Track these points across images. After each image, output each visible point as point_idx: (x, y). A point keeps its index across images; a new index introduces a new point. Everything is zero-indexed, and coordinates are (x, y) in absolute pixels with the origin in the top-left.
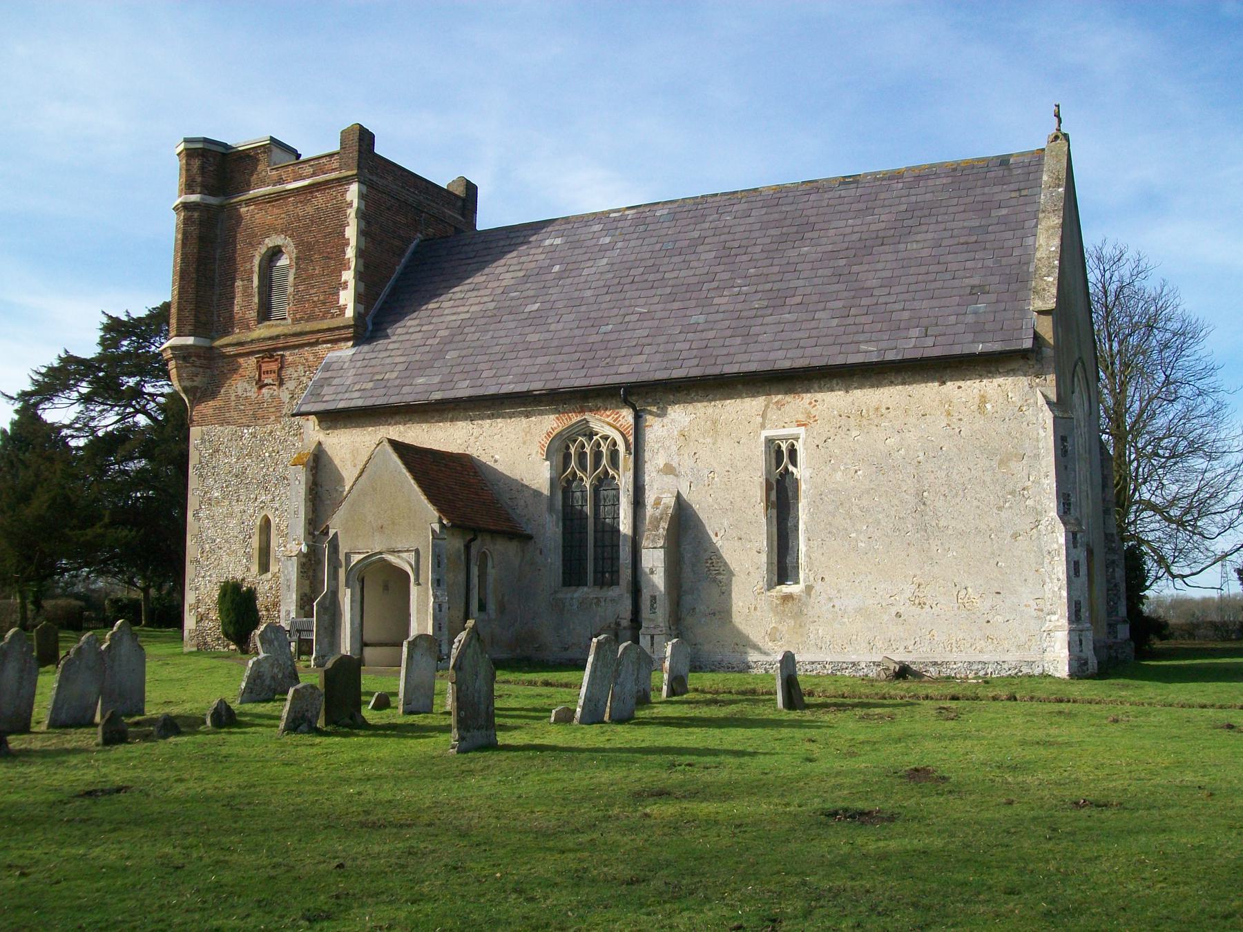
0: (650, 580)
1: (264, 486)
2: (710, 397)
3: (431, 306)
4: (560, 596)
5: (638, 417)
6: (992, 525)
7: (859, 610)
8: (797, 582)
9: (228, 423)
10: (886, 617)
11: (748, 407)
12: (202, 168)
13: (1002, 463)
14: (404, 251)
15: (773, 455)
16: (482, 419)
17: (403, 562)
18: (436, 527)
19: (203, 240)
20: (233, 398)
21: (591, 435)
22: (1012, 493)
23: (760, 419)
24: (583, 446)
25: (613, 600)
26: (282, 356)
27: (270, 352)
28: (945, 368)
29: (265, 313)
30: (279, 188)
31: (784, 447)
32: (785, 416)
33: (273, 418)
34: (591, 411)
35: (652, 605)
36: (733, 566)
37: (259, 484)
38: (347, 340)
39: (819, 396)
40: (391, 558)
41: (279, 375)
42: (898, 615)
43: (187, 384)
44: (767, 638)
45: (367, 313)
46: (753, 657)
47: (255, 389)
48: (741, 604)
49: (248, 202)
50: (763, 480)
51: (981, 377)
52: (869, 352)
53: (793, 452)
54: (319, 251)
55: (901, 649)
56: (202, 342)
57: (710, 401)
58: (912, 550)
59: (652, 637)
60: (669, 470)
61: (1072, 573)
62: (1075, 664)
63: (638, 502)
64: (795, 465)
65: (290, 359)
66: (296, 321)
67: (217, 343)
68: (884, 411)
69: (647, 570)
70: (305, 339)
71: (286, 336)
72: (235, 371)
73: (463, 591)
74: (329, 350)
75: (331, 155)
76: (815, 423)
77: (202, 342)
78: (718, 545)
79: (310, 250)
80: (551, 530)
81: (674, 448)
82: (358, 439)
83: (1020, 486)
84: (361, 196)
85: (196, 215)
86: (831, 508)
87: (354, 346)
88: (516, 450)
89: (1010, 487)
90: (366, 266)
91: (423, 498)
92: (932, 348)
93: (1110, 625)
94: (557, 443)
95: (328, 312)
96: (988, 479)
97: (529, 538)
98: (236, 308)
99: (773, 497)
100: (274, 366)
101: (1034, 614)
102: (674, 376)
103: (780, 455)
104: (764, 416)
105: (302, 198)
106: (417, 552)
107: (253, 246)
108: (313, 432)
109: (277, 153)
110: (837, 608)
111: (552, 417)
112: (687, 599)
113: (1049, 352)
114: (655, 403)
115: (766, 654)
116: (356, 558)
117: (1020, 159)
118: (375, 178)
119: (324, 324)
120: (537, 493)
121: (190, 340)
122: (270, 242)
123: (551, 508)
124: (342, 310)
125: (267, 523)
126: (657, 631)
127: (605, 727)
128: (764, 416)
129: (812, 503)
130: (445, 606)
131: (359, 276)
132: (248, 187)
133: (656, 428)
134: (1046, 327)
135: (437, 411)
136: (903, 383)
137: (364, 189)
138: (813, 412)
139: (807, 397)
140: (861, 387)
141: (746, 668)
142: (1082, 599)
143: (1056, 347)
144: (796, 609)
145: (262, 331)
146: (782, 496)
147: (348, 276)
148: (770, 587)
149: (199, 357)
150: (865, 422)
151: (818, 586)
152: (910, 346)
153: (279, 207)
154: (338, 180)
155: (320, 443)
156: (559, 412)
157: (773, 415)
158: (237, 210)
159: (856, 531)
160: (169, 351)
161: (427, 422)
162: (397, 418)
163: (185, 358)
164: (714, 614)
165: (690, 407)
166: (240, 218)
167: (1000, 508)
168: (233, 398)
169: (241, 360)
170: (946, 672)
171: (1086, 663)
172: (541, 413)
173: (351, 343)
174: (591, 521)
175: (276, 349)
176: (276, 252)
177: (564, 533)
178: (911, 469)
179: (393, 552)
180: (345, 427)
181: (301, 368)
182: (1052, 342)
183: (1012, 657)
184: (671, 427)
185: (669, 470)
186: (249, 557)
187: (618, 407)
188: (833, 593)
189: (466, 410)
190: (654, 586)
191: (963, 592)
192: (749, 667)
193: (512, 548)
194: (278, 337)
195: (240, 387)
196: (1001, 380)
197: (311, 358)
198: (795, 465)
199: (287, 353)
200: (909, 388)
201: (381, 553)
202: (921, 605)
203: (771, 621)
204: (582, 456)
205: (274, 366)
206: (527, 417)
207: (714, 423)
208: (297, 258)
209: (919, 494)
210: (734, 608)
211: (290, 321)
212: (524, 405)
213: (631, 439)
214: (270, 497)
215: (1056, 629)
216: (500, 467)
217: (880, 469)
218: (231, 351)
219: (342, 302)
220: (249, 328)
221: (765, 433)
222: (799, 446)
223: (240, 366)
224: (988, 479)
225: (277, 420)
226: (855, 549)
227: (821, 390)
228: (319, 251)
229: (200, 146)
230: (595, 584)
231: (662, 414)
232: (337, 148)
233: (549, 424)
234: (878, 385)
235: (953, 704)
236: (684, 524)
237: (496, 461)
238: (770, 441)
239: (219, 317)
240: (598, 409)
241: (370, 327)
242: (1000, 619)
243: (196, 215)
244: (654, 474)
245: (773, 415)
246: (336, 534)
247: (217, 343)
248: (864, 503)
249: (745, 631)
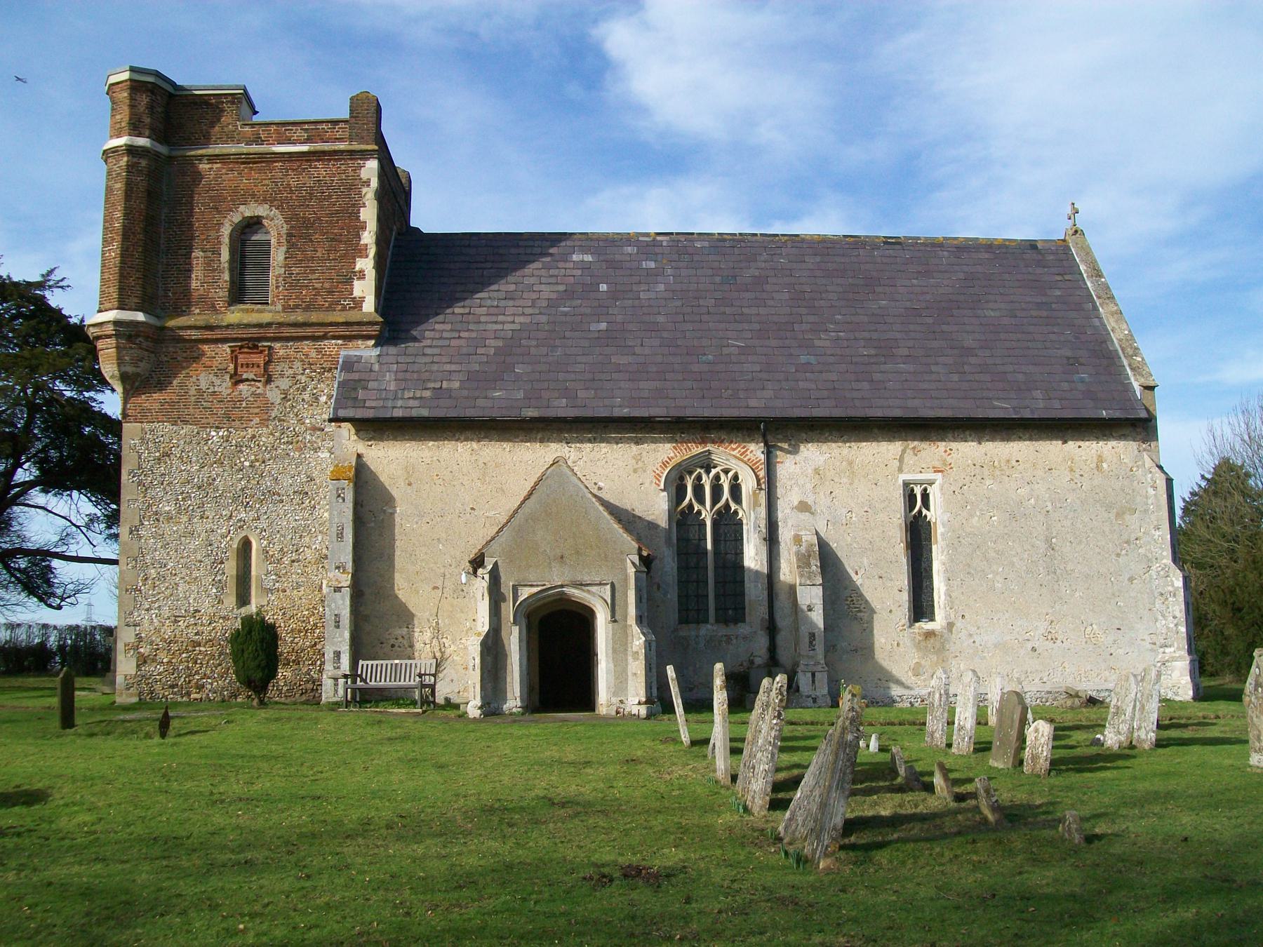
0: (807, 617)
1: (241, 499)
2: (845, 437)
4: (681, 634)
8: (932, 619)
9: (186, 422)
11: (888, 450)
12: (151, 107)
13: (1118, 515)
16: (582, 442)
19: (152, 195)
20: (192, 392)
22: (1128, 542)
24: (699, 478)
25: (745, 638)
26: (270, 348)
27: (251, 342)
29: (238, 294)
30: (255, 148)
31: (918, 491)
32: (926, 461)
33: (257, 420)
34: (714, 442)
35: (811, 643)
36: (875, 604)
37: (235, 499)
39: (954, 445)
41: (266, 370)
42: (1034, 649)
43: (130, 369)
44: (910, 674)
46: (896, 691)
47: (228, 382)
48: (883, 640)
49: (212, 158)
51: (1098, 439)
52: (1002, 408)
53: (925, 496)
55: (1037, 681)
56: (153, 321)
57: (845, 442)
59: (813, 675)
60: (804, 507)
63: (772, 539)
64: (928, 509)
65: (282, 352)
66: (286, 308)
67: (172, 323)
68: (1014, 463)
69: (805, 608)
70: (309, 331)
71: (281, 325)
72: (197, 359)
75: (335, 122)
76: (956, 474)
77: (153, 321)
78: (858, 583)
79: (307, 228)
81: (809, 486)
82: (414, 454)
83: (1133, 537)
85: (144, 163)
87: (375, 345)
89: (1125, 537)
92: (1058, 410)
95: (338, 303)
96: (1107, 529)
98: (194, 284)
100: (260, 360)
101: (1149, 646)
102: (814, 415)
104: (901, 460)
105: (295, 166)
106: (613, 586)
107: (219, 212)
108: (348, 441)
110: (977, 643)
111: (668, 446)
115: (908, 688)
116: (525, 593)
117: (1047, 246)
119: (339, 317)
121: (140, 317)
122: (248, 211)
124: (358, 303)
125: (246, 545)
126: (819, 668)
128: (901, 460)
129: (953, 546)
132: (206, 140)
133: (787, 464)
135: (522, 429)
136: (1031, 439)
138: (949, 459)
139: (942, 445)
140: (993, 440)
141: (891, 702)
144: (938, 645)
145: (235, 315)
146: (918, 536)
147: (366, 264)
149: (147, 338)
150: (997, 473)
151: (959, 624)
152: (1037, 406)
153: (260, 171)
154: (352, 152)
155: (359, 456)
156: (676, 441)
157: (909, 459)
158: (193, 165)
159: (993, 572)
160: (111, 327)
161: (509, 440)
162: (469, 434)
163: (130, 338)
164: (856, 651)
165: (825, 447)
166: (198, 176)
167: (1118, 555)
168: (192, 392)
169: (205, 347)
172: (655, 441)
173: (373, 342)
174: (710, 557)
179: (580, 585)
180: (395, 439)
181: (298, 364)
184: (807, 467)
185: (804, 507)
186: (221, 586)
187: (744, 441)
188: (973, 630)
189: (560, 430)
191: (1089, 629)
192: (894, 701)
194: (269, 325)
195: (206, 379)
196: (1113, 443)
197: (313, 354)
198: (928, 509)
199: (277, 345)
200: (1036, 444)
201: (562, 586)
202: (1054, 640)
203: (913, 657)
204: (699, 490)
205: (260, 360)
206: (637, 443)
207: (851, 463)
208: (289, 235)
209: (1048, 541)
210: (877, 645)
211: (279, 307)
212: (634, 431)
213: (762, 474)
214: (252, 514)
215: (1174, 659)
217: (1013, 517)
218: (195, 334)
219: (357, 292)
222: (934, 492)
223: (203, 354)
224: (1107, 529)
225: (264, 422)
227: (955, 440)
229: (150, 79)
230: (717, 621)
231: (794, 451)
232: (345, 115)
233: (662, 454)
236: (827, 562)
237: (600, 489)
239: (166, 290)
240: (722, 442)
242: (1121, 651)
243: (144, 163)
244: (788, 511)
245: (909, 459)
246: (496, 564)
247: (172, 323)
249: (888, 668)
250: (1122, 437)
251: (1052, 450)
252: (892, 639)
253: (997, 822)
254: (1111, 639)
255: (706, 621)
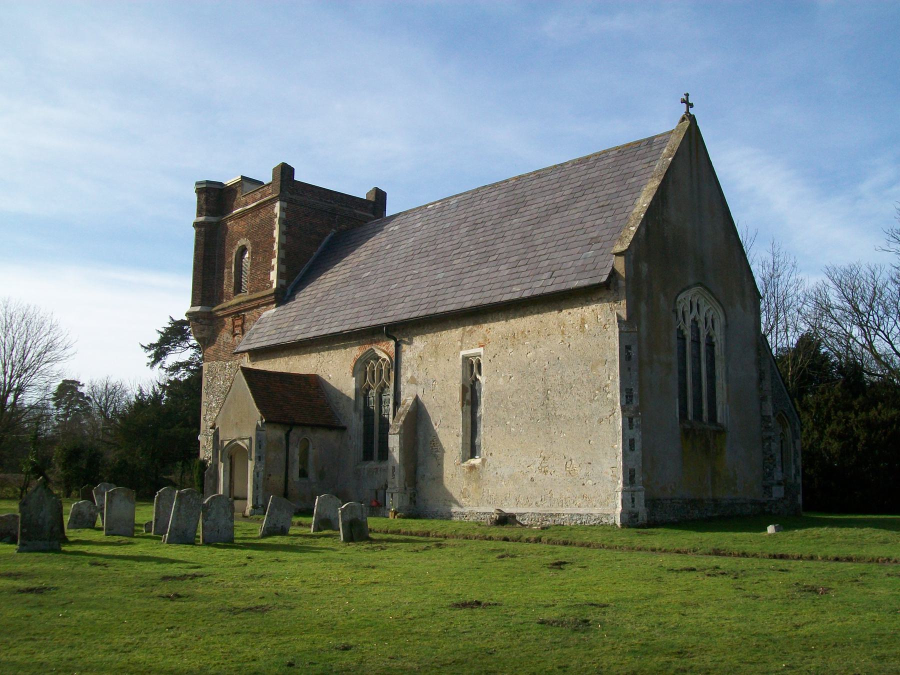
3: (322, 277)
4: (359, 467)
5: (398, 346)
6: (587, 413)
7: (510, 476)
10: (525, 481)
11: (454, 335)
12: (207, 200)
14: (321, 241)
15: (469, 368)
17: (244, 444)
18: (259, 422)
21: (377, 358)
23: (459, 344)
27: (238, 314)
28: (562, 300)
29: (238, 289)
36: (445, 446)
38: (272, 303)
39: (492, 325)
40: (240, 443)
42: (532, 479)
45: (288, 285)
50: (460, 385)
51: (582, 305)
53: (479, 365)
54: (262, 249)
56: (206, 309)
57: (435, 332)
58: (541, 433)
60: (413, 381)
61: (628, 448)
62: (626, 517)
64: (480, 374)
66: (251, 292)
73: (284, 464)
74: (265, 310)
77: (206, 309)
78: (438, 430)
80: (355, 423)
81: (416, 366)
83: (603, 383)
84: (282, 209)
85: (203, 229)
86: (496, 404)
88: (337, 370)
90: (287, 254)
91: (254, 404)
93: (765, 487)
94: (359, 366)
96: (585, 380)
97: (344, 429)
99: (468, 397)
100: (239, 322)
103: (472, 367)
105: (254, 214)
109: (246, 184)
111: (357, 348)
112: (421, 469)
113: (622, 283)
114: (407, 336)
115: (461, 507)
118: (294, 197)
120: (349, 399)
123: (356, 409)
124: (271, 283)
127: (197, 548)
130: (261, 474)
131: (281, 261)
134: (620, 265)
136: (538, 313)
137: (285, 205)
140: (514, 318)
141: (449, 516)
142: (636, 467)
143: (627, 280)
146: (471, 396)
147: (274, 262)
148: (464, 460)
149: (204, 318)
154: (270, 200)
161: (298, 354)
167: (591, 401)
169: (226, 319)
170: (559, 521)
171: (636, 516)
175: (241, 311)
176: (243, 250)
177: (364, 425)
178: (541, 375)
180: (329, 349)
182: (624, 275)
183: (596, 511)
184: (416, 349)
185: (413, 381)
189: (317, 345)
190: (394, 460)
193: (332, 436)
195: (225, 336)
196: (593, 306)
198: (480, 374)
201: (235, 440)
206: (345, 348)
209: (546, 392)
210: (445, 475)
216: (332, 383)
218: (220, 313)
220: (230, 299)
221: (464, 353)
224: (585, 380)
226: (509, 432)
228: (262, 249)
229: (204, 186)
231: (410, 343)
233: (356, 352)
234: (523, 315)
235: (506, 545)
236: (418, 416)
238: (466, 359)
241: (283, 297)
243: (203, 229)
248: (515, 399)
250: (600, 300)
251: (550, 318)
252: (453, 471)
253: (770, 535)
254: (583, 472)
255: (372, 459)
